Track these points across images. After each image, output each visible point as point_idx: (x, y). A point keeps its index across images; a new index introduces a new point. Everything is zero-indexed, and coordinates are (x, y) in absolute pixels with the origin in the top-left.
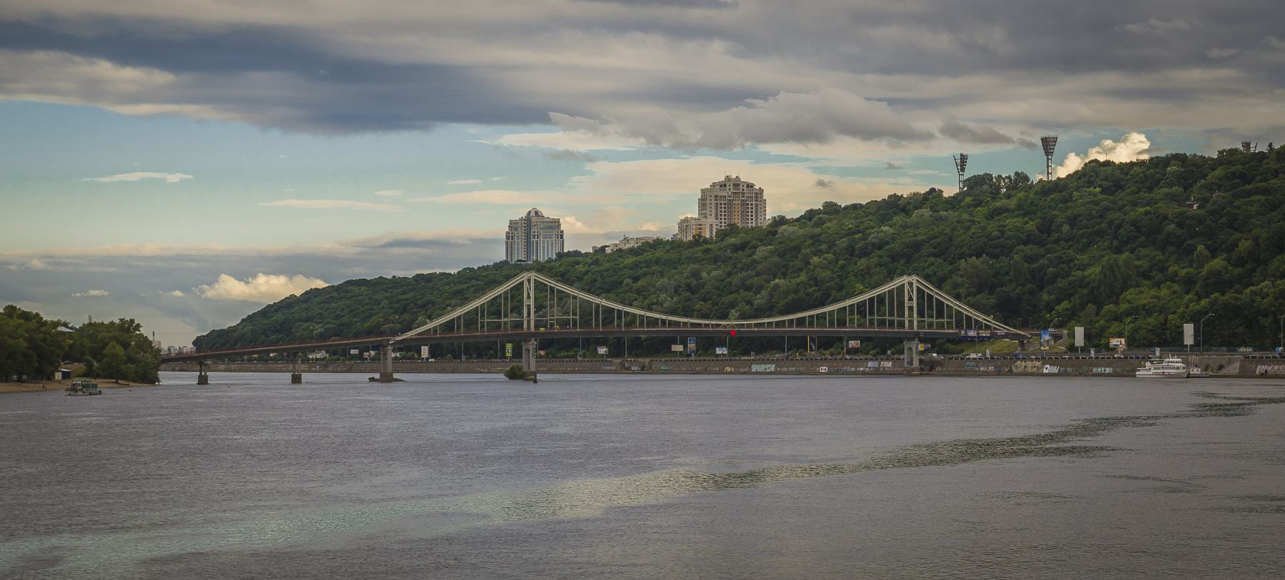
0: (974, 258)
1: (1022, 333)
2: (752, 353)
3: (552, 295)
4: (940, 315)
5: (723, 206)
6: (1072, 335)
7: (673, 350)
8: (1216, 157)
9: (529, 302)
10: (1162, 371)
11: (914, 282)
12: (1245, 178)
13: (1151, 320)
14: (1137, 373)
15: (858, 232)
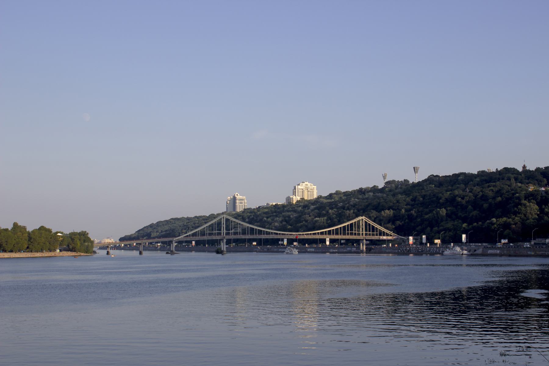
0: (387, 210)
1: (404, 238)
3: (358, 224)
4: (377, 231)
6: (421, 239)
7: (345, 241)
8: (476, 174)
10: (453, 252)
11: (364, 220)
12: (487, 181)
13: (451, 233)
15: (346, 201)
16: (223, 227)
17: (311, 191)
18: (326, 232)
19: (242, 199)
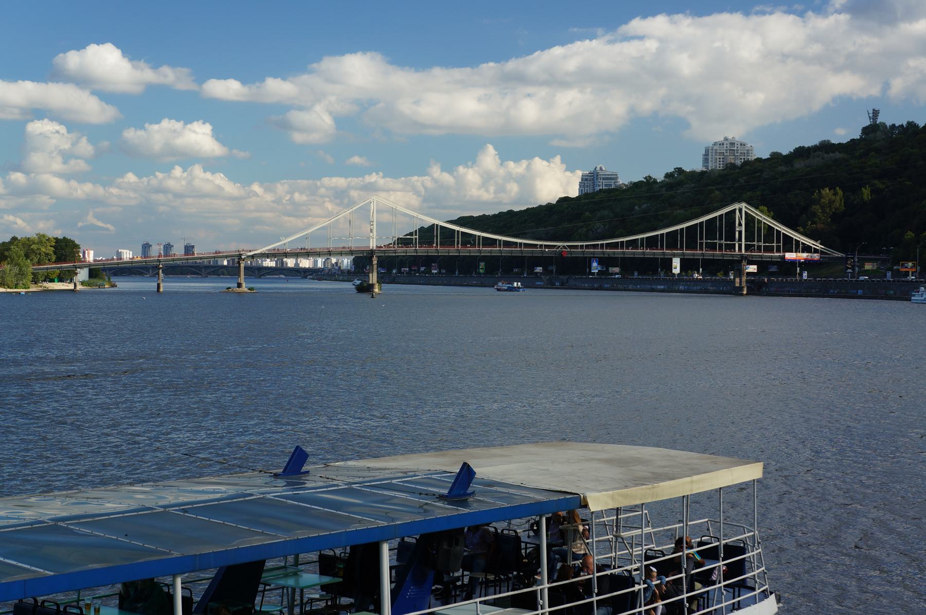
2: (23, 293)
5: (721, 160)
9: (741, 228)
11: (744, 210)
14: (913, 298)
16: (740, 232)
17: (742, 157)
18: (622, 242)
19: (610, 176)
